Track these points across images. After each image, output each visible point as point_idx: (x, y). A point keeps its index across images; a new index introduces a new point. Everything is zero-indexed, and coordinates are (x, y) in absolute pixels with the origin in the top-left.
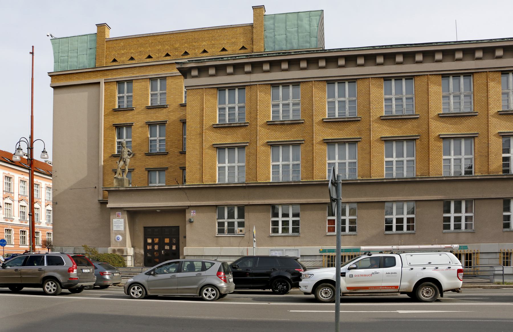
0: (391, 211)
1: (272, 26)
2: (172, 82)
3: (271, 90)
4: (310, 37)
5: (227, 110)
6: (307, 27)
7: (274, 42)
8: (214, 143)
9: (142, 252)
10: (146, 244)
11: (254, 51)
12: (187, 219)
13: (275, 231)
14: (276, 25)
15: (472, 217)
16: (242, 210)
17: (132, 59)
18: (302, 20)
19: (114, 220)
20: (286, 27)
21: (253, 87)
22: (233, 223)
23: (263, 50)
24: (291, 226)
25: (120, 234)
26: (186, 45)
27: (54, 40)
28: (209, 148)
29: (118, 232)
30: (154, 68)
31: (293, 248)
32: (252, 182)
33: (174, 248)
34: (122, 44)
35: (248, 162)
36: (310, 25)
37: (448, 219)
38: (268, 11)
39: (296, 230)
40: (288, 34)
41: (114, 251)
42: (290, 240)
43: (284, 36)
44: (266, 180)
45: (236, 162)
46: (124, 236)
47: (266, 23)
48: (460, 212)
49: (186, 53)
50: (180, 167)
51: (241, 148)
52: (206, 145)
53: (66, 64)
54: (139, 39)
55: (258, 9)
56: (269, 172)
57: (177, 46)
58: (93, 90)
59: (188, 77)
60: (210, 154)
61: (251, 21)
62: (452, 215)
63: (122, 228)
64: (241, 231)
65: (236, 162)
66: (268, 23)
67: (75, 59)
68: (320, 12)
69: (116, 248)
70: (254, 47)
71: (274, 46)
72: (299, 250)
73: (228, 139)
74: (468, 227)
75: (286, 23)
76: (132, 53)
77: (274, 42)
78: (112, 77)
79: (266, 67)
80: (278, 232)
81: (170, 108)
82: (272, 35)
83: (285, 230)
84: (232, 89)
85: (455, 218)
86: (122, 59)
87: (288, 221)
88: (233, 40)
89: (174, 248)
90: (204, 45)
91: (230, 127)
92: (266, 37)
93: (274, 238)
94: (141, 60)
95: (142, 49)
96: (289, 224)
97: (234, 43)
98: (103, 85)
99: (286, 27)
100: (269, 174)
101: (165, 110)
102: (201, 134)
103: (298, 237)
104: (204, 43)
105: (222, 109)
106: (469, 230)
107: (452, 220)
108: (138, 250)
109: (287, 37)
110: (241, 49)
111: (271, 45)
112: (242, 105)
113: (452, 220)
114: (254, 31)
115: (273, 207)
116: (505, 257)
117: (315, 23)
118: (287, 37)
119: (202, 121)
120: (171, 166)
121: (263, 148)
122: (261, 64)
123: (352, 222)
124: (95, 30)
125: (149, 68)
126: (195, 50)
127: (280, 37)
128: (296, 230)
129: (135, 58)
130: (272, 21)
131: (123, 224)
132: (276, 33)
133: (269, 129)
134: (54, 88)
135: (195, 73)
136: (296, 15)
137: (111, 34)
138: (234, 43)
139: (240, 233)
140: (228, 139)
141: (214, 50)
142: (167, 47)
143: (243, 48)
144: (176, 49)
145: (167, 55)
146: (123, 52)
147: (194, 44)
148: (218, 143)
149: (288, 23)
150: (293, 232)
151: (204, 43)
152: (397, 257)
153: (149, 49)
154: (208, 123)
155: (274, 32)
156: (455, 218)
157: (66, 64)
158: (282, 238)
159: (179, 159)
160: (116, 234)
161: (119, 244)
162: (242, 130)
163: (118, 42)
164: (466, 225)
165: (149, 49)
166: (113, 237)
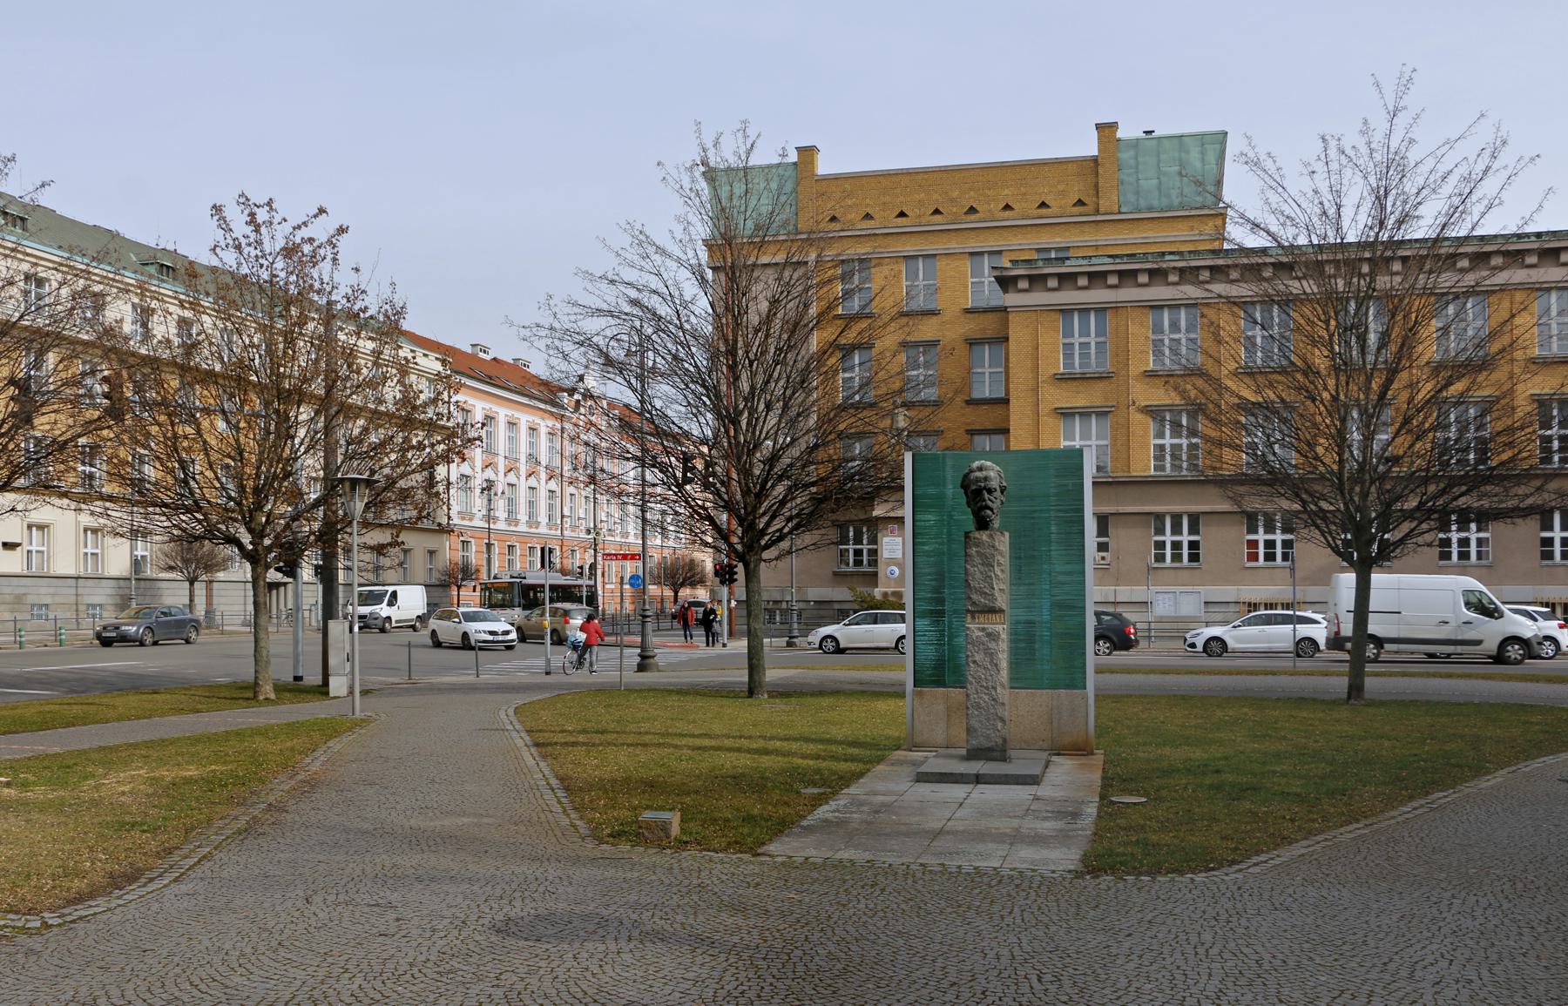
0: (94, 756)
1: (1132, 162)
2: (947, 264)
3: (1150, 317)
5: (1077, 347)
6: (1198, 164)
7: (1137, 193)
8: (1056, 406)
11: (1102, 210)
13: (1160, 558)
14: (1140, 159)
15: (1488, 539)
17: (868, 216)
18: (1188, 152)
19: (886, 540)
20: (1158, 165)
21: (1120, 311)
22: (862, 550)
23: (1116, 209)
24: (1279, 551)
25: (895, 565)
26: (972, 193)
28: (1048, 415)
29: (892, 561)
31: (1190, 588)
32: (1121, 475)
35: (1114, 440)
36: (1203, 161)
39: (1194, 557)
40: (1164, 179)
41: (885, 595)
42: (1185, 574)
43: (1155, 182)
44: (1145, 471)
45: (1094, 438)
46: (901, 566)
47: (1119, 155)
48: (1180, 533)
49: (972, 210)
50: (967, 431)
51: (1102, 414)
52: (1045, 408)
54: (880, 179)
55: (1106, 130)
56: (1149, 456)
57: (955, 194)
59: (1010, 289)
61: (1094, 152)
62: (1168, 538)
63: (899, 555)
64: (1103, 558)
65: (1094, 438)
66: (1126, 156)
68: (1221, 136)
69: (890, 590)
70: (1101, 202)
71: (1138, 200)
72: (1202, 593)
73: (1080, 398)
74: (1484, 556)
75: (1158, 156)
76: (867, 205)
77: (1137, 193)
79: (1143, 279)
81: (947, 316)
82: (1132, 179)
83: (1177, 557)
84: (1084, 311)
85: (869, 550)
86: (849, 217)
87: (1164, 542)
88: (1061, 187)
90: (1007, 195)
91: (1083, 378)
92: (1122, 183)
93: (1159, 571)
94: (885, 220)
95: (888, 199)
97: (1063, 193)
99: (1158, 165)
100: (1149, 461)
101: (934, 320)
102: (1036, 390)
103: (1198, 571)
104: (1006, 192)
105: (1068, 347)
106: (1484, 562)
107: (1261, 545)
109: (1160, 183)
110: (1074, 205)
111: (1132, 198)
112: (1102, 339)
113: (1261, 545)
114: (1100, 171)
115: (1159, 517)
118: (1160, 183)
120: (949, 429)
122: (1134, 273)
123: (1194, 545)
125: (904, 238)
126: (990, 205)
127: (1149, 184)
128: (1194, 557)
129: (875, 216)
130: (1132, 153)
131: (901, 547)
132: (1140, 176)
133: (1148, 384)
135: (1023, 284)
136: (1176, 141)
138: (1063, 193)
139: (1102, 562)
140: (1080, 398)
141: (1024, 205)
142: (935, 196)
143: (1080, 203)
144: (952, 200)
145: (937, 212)
147: (987, 191)
148: (1064, 406)
149: (1163, 157)
150: (1190, 561)
151: (1006, 192)
152: (1290, 563)
153: (902, 199)
154: (1046, 370)
155: (1137, 172)
158: (1171, 571)
159: (964, 415)
160: (888, 565)
161: (893, 582)
162: (1100, 385)
163: (839, 182)
164: (1479, 553)
165: (902, 199)
166: (882, 569)
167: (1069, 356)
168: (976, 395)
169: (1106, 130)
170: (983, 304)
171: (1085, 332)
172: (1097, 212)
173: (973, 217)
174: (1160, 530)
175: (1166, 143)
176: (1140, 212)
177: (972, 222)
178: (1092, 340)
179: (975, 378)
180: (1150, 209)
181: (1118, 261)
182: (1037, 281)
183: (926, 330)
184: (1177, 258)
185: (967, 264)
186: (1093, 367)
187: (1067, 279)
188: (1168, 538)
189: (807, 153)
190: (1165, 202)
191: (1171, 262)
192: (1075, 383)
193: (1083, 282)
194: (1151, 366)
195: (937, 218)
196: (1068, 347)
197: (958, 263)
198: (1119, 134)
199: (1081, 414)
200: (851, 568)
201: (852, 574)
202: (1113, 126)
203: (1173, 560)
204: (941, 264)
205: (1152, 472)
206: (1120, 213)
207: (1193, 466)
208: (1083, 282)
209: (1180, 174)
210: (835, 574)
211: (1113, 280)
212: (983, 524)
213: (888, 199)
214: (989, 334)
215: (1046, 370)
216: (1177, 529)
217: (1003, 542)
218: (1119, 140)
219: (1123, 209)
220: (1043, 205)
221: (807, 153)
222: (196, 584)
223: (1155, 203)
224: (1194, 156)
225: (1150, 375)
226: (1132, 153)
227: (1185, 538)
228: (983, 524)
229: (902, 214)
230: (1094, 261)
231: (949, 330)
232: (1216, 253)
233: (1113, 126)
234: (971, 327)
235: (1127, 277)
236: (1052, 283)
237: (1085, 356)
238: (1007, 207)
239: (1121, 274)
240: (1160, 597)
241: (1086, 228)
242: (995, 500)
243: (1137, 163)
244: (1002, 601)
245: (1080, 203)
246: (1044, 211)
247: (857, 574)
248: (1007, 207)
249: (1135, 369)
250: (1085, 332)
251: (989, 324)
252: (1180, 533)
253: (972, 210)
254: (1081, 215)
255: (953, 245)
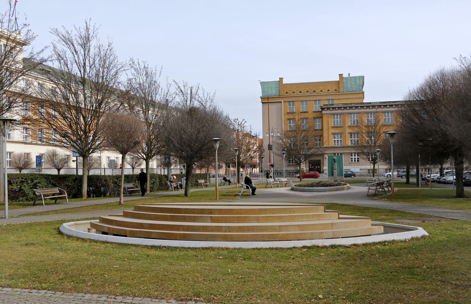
4: (360, 87)
6: (359, 83)
7: (347, 88)
9: (308, 169)
10: (309, 166)
11: (340, 91)
12: (324, 157)
13: (352, 161)
16: (341, 154)
17: (294, 92)
18: (356, 80)
23: (343, 91)
27: (263, 84)
30: (303, 97)
32: (344, 145)
33: (319, 167)
34: (289, 86)
37: (352, 158)
38: (344, 76)
39: (358, 161)
42: (354, 164)
43: (350, 86)
48: (356, 156)
53: (267, 93)
55: (341, 75)
57: (311, 88)
58: (279, 104)
60: (331, 137)
61: (338, 80)
62: (353, 157)
66: (345, 81)
67: (271, 92)
73: (337, 131)
75: (351, 81)
77: (347, 88)
78: (286, 100)
80: (352, 161)
83: (355, 161)
84: (337, 114)
86: (290, 92)
89: (319, 167)
90: (322, 88)
91: (337, 127)
94: (297, 93)
95: (298, 89)
96: (142, 223)
97: (332, 88)
98: (283, 102)
101: (307, 114)
102: (328, 129)
108: (307, 168)
111: (346, 89)
114: (340, 84)
116: (354, 156)
117: (361, 81)
119: (328, 125)
121: (348, 134)
124: (279, 80)
127: (349, 86)
130: (346, 80)
134: (262, 103)
135: (326, 109)
137: (284, 82)
140: (337, 131)
142: (307, 88)
143: (336, 90)
144: (311, 89)
145: (307, 92)
146: (290, 89)
149: (352, 81)
154: (330, 126)
156: (357, 158)
157: (267, 93)
162: (340, 128)
167: (334, 123)
168: (315, 129)
169: (341, 75)
170: (317, 110)
171: (337, 118)
172: (339, 92)
173: (315, 93)
174: (352, 156)
175: (352, 78)
176: (347, 92)
177: (315, 94)
178: (339, 120)
179: (315, 125)
180: (349, 91)
181: (343, 105)
182: (328, 109)
183: (306, 115)
184: (354, 104)
185: (314, 102)
186: (339, 125)
187: (334, 108)
188: (353, 157)
189: (281, 79)
190: (352, 90)
191: (353, 105)
192: (336, 128)
193: (337, 109)
194: (350, 125)
195: (308, 93)
196: (334, 121)
197: (312, 102)
198: (343, 76)
199: (337, 134)
200: (291, 164)
201: (291, 165)
202: (342, 75)
203: (354, 161)
204: (309, 102)
205: (350, 145)
206: (343, 92)
207: (358, 144)
208: (337, 109)
209: (355, 84)
210: (288, 165)
211: (342, 109)
212: (335, 162)
213: (298, 89)
214: (318, 116)
215: (330, 126)
216: (355, 156)
217: (336, 164)
218: (343, 77)
219: (344, 92)
220: (328, 90)
221: (281, 79)
222: (165, 170)
223: (350, 90)
224: (358, 81)
225: (349, 127)
226: (346, 80)
227: (356, 157)
228: (335, 162)
229: (300, 92)
230: (339, 105)
231: (310, 116)
232: (361, 103)
233: (342, 75)
234: (314, 115)
235: (345, 108)
236: (331, 109)
237: (337, 123)
238: (321, 91)
239: (344, 107)
240: (352, 168)
241: (337, 95)
242: (336, 160)
243: (347, 82)
244: (337, 169)
245: (336, 90)
246: (329, 92)
247: (293, 165)
248: (321, 91)
249: (347, 125)
250: (337, 118)
251: (318, 114)
252: (356, 156)
253: (314, 91)
254: (336, 93)
255: (311, 99)
